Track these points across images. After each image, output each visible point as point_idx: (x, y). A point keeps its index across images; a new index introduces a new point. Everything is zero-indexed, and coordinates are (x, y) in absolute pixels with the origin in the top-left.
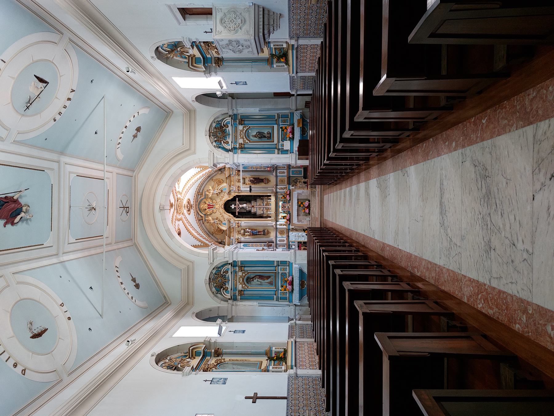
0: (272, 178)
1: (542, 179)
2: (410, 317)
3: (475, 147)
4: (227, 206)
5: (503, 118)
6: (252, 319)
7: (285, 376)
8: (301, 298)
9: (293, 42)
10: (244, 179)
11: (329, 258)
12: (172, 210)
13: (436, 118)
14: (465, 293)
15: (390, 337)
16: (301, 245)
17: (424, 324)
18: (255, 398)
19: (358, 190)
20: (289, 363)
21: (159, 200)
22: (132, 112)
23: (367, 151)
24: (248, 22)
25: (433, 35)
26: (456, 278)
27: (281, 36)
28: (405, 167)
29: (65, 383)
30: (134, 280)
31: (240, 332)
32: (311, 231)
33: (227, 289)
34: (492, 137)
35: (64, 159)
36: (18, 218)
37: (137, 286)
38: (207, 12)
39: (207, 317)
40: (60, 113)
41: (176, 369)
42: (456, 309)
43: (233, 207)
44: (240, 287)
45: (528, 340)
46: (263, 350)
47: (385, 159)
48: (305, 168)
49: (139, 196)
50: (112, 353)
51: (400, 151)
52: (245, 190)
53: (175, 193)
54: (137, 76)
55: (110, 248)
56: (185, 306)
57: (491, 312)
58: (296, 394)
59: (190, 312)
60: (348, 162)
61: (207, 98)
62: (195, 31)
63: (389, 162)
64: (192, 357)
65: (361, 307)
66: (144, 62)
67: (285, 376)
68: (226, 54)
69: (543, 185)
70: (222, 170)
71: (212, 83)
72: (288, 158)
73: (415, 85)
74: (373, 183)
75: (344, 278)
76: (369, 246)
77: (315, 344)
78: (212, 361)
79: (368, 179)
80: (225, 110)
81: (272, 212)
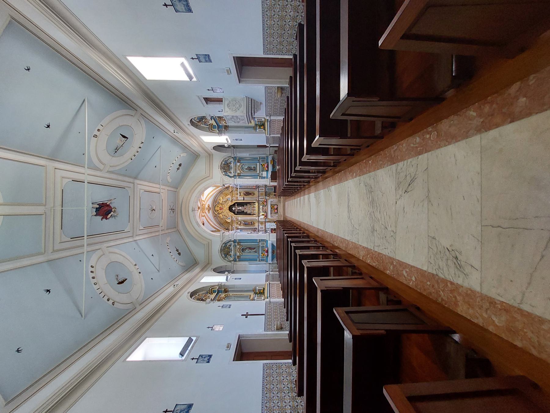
0: (256, 192)
1: (400, 193)
2: (332, 269)
3: (365, 176)
4: (230, 208)
5: (380, 160)
6: (245, 272)
7: (264, 302)
8: (272, 260)
9: (268, 118)
10: (240, 193)
11: (288, 237)
12: (199, 210)
13: (345, 160)
14: (361, 255)
15: (321, 280)
16: (273, 230)
17: (339, 271)
18: (247, 315)
19: (304, 199)
20: (266, 295)
21: (191, 205)
22: (177, 156)
23: (309, 178)
24: (242, 106)
25: (343, 115)
26: (356, 247)
27: (261, 114)
28: (329, 186)
29: (137, 309)
30: (177, 250)
31: (238, 279)
32: (278, 222)
33: (230, 255)
34: (374, 171)
35: (137, 182)
36: (110, 215)
37: (179, 254)
38: (220, 100)
39: (219, 271)
40: (134, 156)
41: (202, 300)
42: (356, 263)
43: (234, 209)
44: (238, 254)
45: (394, 279)
46: (251, 289)
47: (318, 182)
48: (275, 187)
49: (180, 202)
50: (165, 292)
51: (326, 178)
52: (240, 199)
53: (201, 201)
54: (180, 135)
55: (163, 232)
56: (205, 266)
57: (374, 264)
58: (269, 312)
59: (210, 269)
60: (298, 184)
61: (219, 148)
62: (213, 110)
63: (321, 184)
64: (211, 293)
65: (306, 263)
66: (184, 127)
67: (264, 302)
68: (230, 124)
69: (401, 196)
70: (227, 188)
71: (222, 139)
72: (266, 181)
73: (334, 142)
74: (312, 195)
75: (296, 248)
76: (310, 230)
77: (280, 285)
78: (223, 295)
79: (309, 193)
80: (229, 154)
81: (256, 212)
